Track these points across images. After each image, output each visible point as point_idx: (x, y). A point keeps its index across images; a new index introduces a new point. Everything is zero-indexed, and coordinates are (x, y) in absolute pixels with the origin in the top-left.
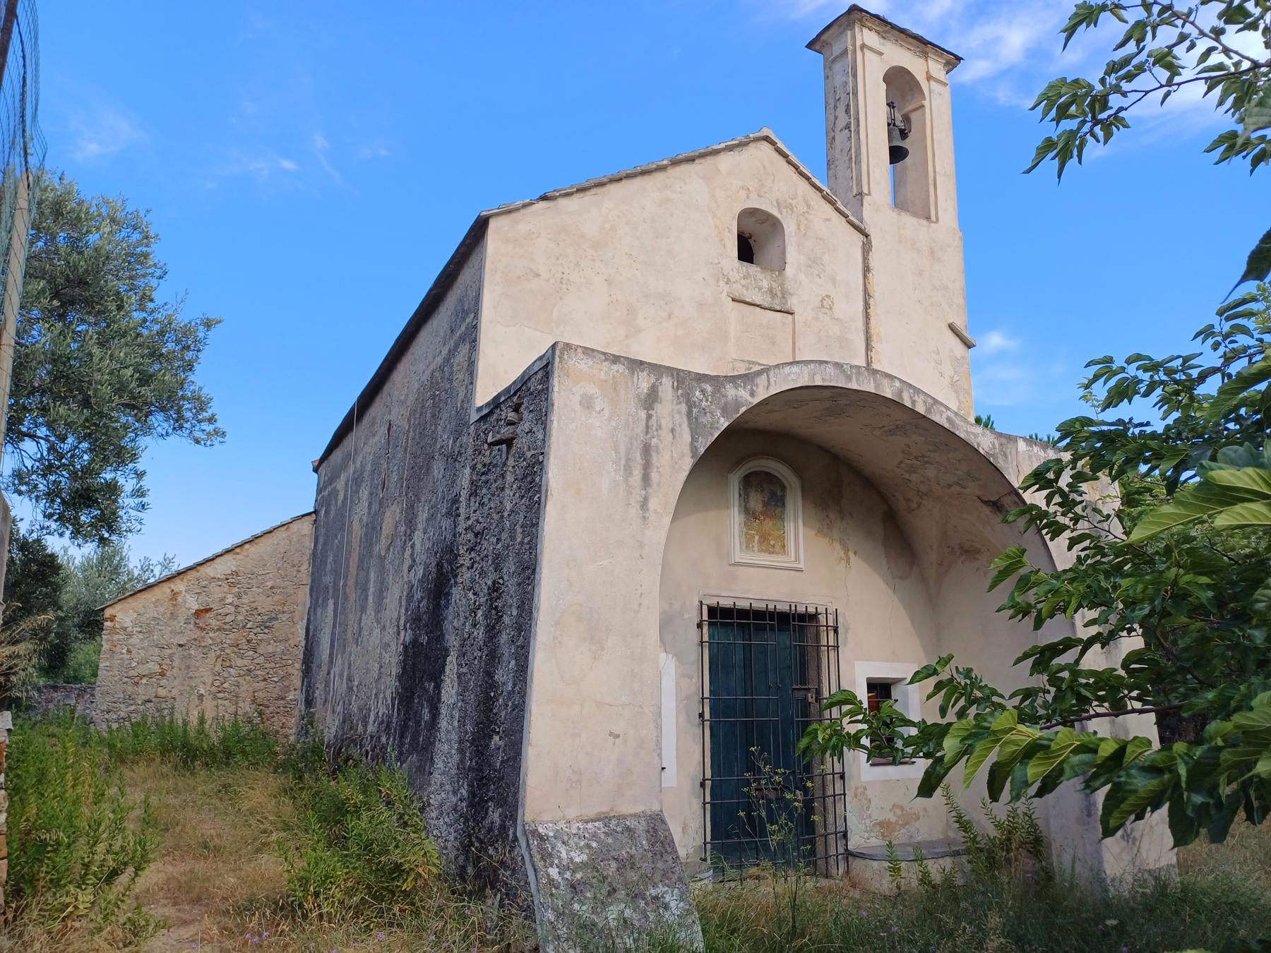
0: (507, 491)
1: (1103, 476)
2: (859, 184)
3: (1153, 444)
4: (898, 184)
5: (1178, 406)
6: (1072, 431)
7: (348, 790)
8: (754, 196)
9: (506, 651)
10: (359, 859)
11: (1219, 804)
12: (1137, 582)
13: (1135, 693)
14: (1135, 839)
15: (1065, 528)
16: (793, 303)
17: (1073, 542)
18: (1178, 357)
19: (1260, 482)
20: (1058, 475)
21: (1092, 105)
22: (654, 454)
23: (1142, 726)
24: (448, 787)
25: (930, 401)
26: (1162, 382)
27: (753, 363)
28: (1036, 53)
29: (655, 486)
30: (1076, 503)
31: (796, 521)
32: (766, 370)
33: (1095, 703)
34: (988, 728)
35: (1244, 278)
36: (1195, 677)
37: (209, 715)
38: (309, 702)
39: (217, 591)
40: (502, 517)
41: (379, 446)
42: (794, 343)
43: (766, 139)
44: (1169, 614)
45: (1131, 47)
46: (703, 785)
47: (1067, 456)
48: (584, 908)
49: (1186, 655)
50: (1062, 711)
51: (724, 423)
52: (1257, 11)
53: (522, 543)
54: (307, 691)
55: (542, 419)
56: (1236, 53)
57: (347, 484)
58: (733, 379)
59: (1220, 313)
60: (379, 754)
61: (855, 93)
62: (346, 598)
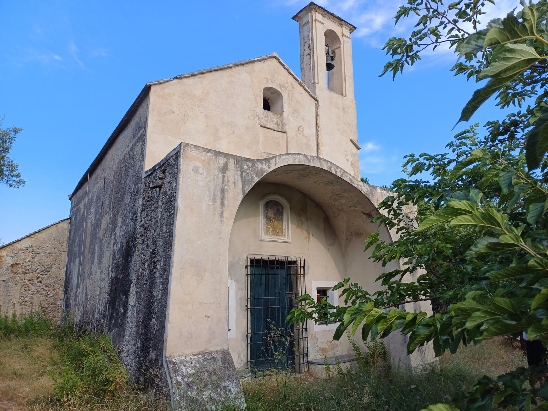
0: (159, 209)
1: (410, 203)
2: (314, 79)
3: (430, 190)
4: (330, 79)
5: (440, 174)
6: (398, 184)
7: (84, 345)
8: (270, 82)
9: (158, 281)
10: (89, 377)
11: (452, 339)
12: (423, 247)
13: (422, 292)
14: (423, 351)
15: (395, 224)
16: (286, 129)
17: (398, 230)
18: (440, 154)
19: (468, 206)
20: (392, 203)
21: (406, 49)
22: (226, 193)
23: (426, 307)
24: (131, 343)
25: (342, 171)
26: (434, 165)
27: (270, 154)
28: (386, 27)
29: (226, 207)
30: (399, 214)
31: (288, 222)
32: (275, 157)
33: (407, 297)
34: (362, 310)
35: (460, 120)
36: (445, 285)
37: (18, 313)
38: (67, 306)
39: (22, 256)
40: (157, 221)
41: (100, 188)
42: (287, 146)
43: (275, 57)
44: (436, 260)
45: (421, 26)
46: (247, 336)
47: (396, 195)
48: (193, 393)
49: (442, 276)
50: (394, 300)
51: (257, 180)
52: (471, 13)
53: (166, 232)
54: (66, 301)
55: (175, 177)
56: (462, 30)
57: (85, 205)
58: (260, 161)
59: (456, 137)
60: (100, 328)
61: (312, 40)
62: (84, 258)
